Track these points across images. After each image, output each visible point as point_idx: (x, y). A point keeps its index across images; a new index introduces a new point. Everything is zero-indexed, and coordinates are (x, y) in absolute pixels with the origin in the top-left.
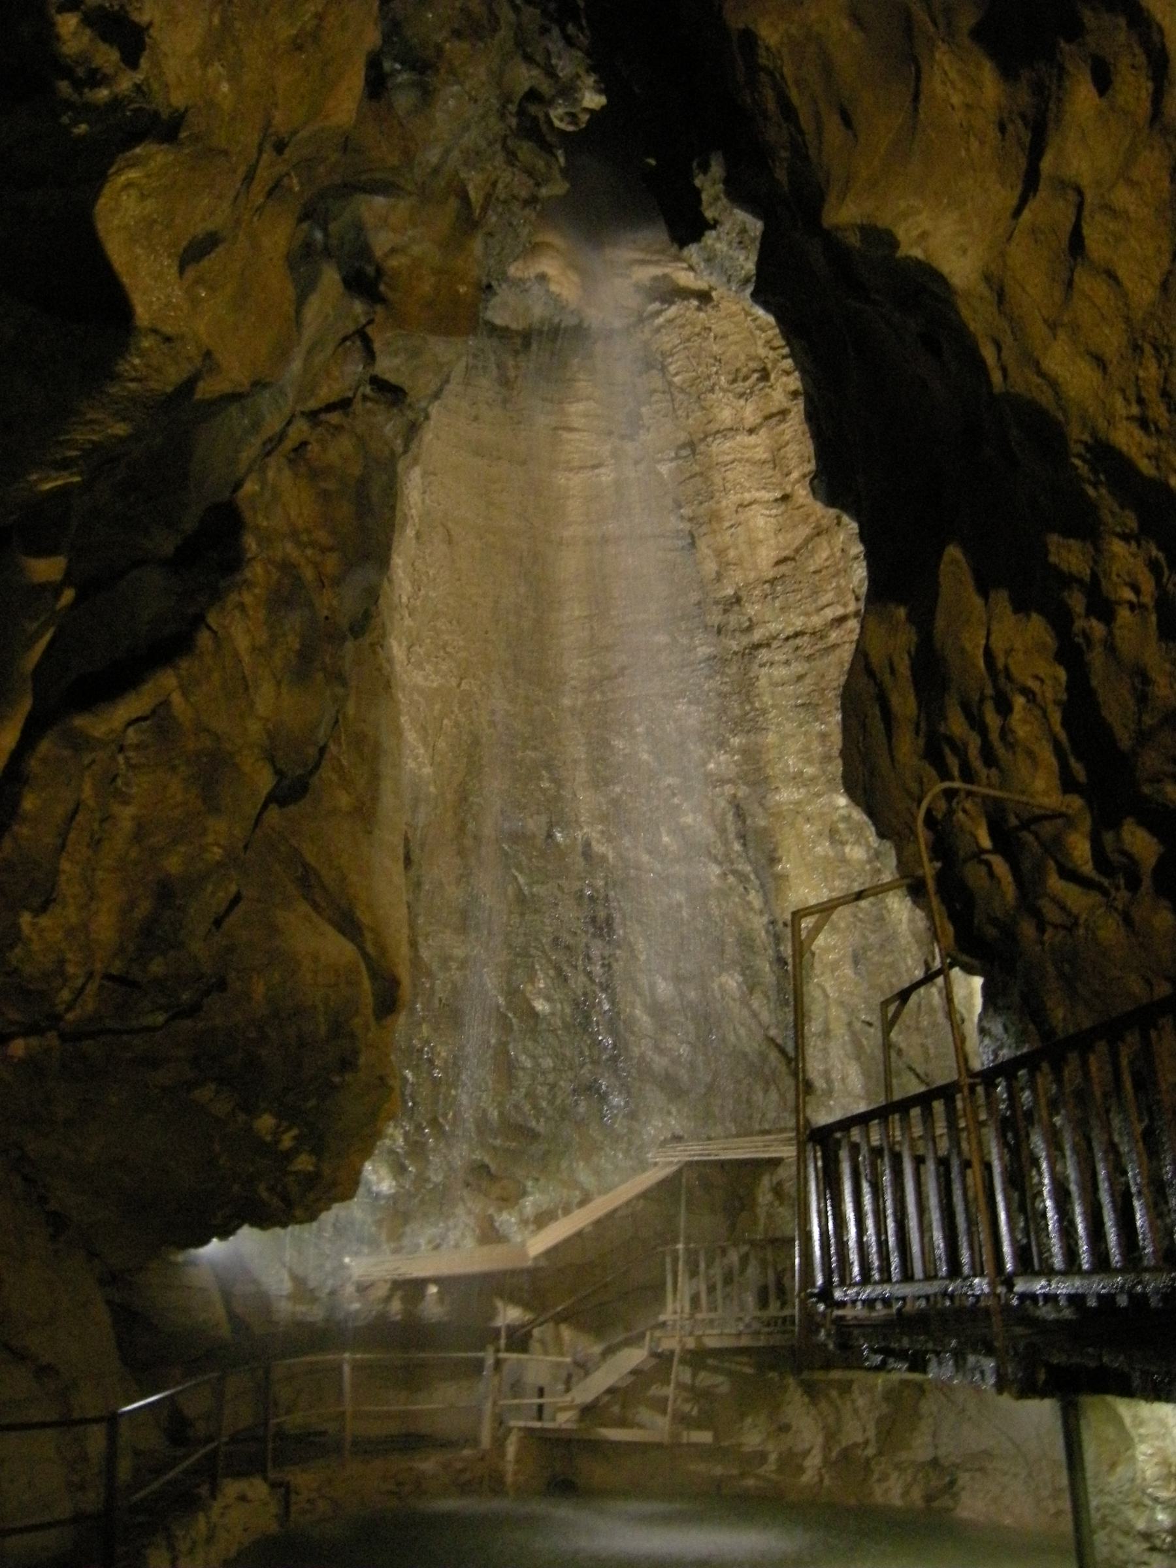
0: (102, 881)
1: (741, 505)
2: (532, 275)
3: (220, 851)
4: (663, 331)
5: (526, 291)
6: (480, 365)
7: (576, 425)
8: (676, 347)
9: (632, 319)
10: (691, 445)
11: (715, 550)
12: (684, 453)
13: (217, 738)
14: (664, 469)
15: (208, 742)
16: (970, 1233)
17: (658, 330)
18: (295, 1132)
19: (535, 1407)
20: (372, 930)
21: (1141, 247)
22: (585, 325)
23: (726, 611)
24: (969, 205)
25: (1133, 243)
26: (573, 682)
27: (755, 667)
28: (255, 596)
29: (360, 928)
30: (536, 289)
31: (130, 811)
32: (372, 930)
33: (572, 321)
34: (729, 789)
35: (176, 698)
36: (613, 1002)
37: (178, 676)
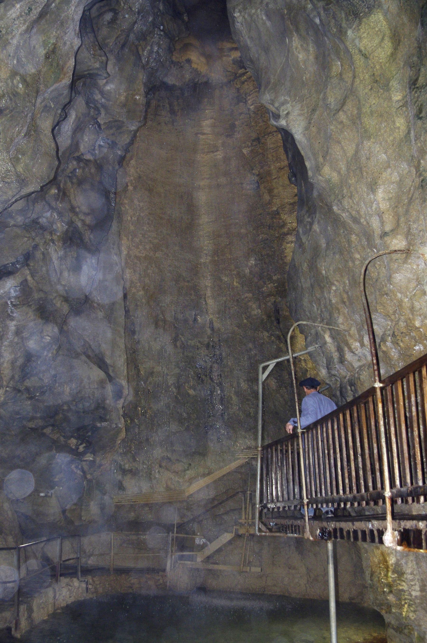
0: (5, 350)
1: (280, 168)
2: (184, 60)
3: (49, 338)
4: (246, 83)
5: (182, 67)
6: (161, 104)
7: (205, 132)
8: (251, 91)
9: (232, 78)
10: (258, 139)
11: (268, 190)
12: (254, 143)
13: (46, 293)
14: (245, 151)
15: (42, 295)
16: (276, 484)
17: (243, 83)
18: (84, 445)
19: (314, 592)
20: (112, 366)
21: (348, 135)
22: (210, 81)
23: (272, 218)
24: (305, 102)
25: (346, 133)
26: (205, 252)
27: (285, 244)
28: (58, 236)
29: (107, 365)
30: (187, 66)
31: (14, 323)
32: (112, 366)
33: (205, 80)
34: (272, 299)
35: (29, 278)
36: (222, 391)
37: (30, 269)
